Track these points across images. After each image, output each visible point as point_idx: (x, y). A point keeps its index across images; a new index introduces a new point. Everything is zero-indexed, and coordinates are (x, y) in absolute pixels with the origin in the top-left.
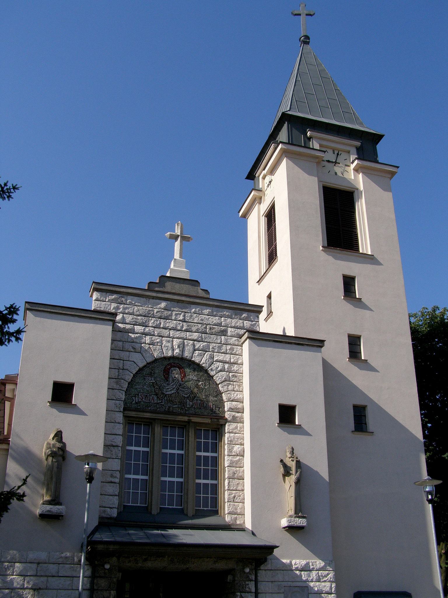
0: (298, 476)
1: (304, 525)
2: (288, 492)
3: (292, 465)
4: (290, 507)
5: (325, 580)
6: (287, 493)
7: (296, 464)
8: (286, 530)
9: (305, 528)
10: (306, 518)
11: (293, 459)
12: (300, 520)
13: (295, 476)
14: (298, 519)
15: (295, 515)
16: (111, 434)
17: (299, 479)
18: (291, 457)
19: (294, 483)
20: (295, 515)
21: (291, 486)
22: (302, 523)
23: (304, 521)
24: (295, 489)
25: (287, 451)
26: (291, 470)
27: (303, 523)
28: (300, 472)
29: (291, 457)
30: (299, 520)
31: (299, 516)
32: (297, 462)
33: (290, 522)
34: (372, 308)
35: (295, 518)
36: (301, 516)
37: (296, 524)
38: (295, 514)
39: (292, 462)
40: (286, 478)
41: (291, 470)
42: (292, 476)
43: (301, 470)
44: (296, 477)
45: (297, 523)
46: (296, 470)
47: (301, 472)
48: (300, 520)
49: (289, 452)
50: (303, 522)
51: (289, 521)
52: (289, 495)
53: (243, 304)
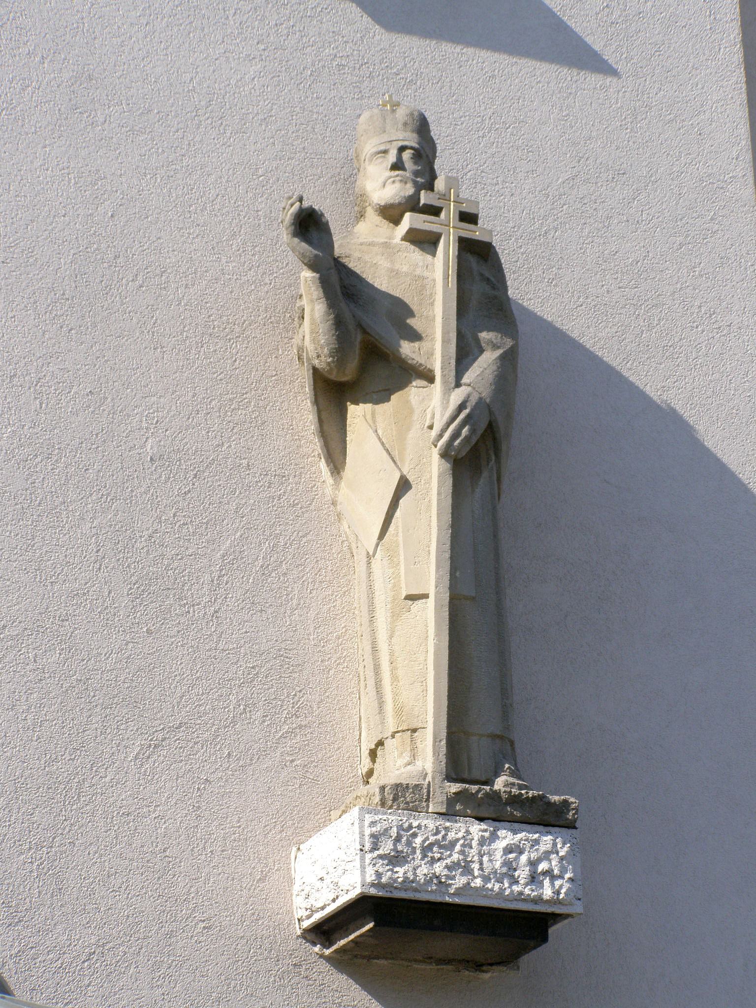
0: (486, 392)
1: (547, 892)
2: (369, 557)
3: (421, 284)
4: (389, 707)
5: (409, 429)
6: (361, 567)
7: (463, 275)
8: (340, 962)
9: (553, 931)
10: (571, 826)
11: (423, 222)
12: (500, 845)
13: (447, 392)
14: (477, 829)
15: (455, 788)
16: (387, 451)
17: (491, 428)
18: (413, 205)
19: (444, 455)
20: (455, 788)
21: (404, 486)
22: (523, 874)
23: (546, 855)
24: (448, 518)
25: (370, 146)
26: (415, 336)
27: (534, 878)
28: (503, 358)
29: (413, 205)
30: (494, 837)
31: (495, 796)
32: (472, 260)
33: (396, 859)
34: (609, 56)
35: (449, 814)
36: (515, 800)
37: (460, 881)
38: (450, 778)
39: (415, 255)
40: (357, 413)
41: (415, 336)
42: (415, 392)
43: (509, 343)
44: (457, 396)
45: (467, 870)
46: (460, 336)
47: (509, 360)
48: (506, 837)
49: (392, 157)
50: (543, 866)
51: (387, 847)
52: (378, 585)
53: (521, 823)
